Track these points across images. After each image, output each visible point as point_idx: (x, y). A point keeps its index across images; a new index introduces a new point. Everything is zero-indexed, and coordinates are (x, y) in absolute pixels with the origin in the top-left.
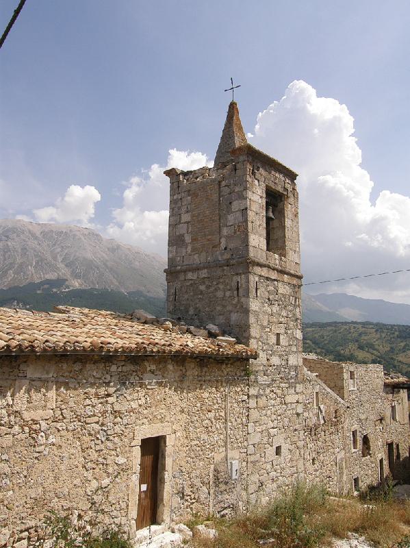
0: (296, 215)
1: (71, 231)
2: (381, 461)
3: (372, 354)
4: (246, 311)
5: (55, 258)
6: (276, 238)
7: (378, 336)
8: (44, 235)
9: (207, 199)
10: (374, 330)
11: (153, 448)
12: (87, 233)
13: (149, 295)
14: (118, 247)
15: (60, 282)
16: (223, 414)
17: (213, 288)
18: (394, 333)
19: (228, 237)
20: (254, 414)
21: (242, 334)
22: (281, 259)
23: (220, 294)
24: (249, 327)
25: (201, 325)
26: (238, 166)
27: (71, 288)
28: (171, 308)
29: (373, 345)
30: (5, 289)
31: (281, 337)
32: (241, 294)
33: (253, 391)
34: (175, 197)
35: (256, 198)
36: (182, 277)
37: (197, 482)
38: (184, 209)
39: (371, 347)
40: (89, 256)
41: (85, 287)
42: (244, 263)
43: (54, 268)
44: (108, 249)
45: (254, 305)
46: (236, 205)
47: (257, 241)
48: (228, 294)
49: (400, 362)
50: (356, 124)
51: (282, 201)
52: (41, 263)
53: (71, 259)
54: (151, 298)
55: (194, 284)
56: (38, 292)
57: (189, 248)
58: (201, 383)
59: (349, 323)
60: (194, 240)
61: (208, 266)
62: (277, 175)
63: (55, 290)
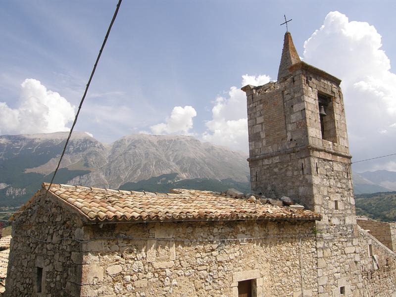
0: (343, 110)
1: (178, 139)
4: (310, 185)
5: (168, 159)
6: (328, 130)
14: (213, 148)
16: (298, 262)
19: (293, 132)
20: (322, 263)
21: (308, 203)
22: (334, 145)
24: (312, 196)
25: (277, 197)
26: (296, 78)
27: (181, 180)
28: (254, 186)
30: (136, 182)
31: (339, 203)
32: (305, 173)
33: (320, 245)
34: (251, 106)
35: (311, 100)
36: (260, 163)
40: (192, 155)
41: (191, 177)
42: (307, 150)
43: (170, 167)
44: (206, 150)
45: (316, 180)
46: (296, 108)
47: (314, 132)
48: (296, 173)
50: (383, 40)
51: (330, 101)
52: (159, 163)
53: (179, 159)
54: (240, 182)
55: (270, 168)
56: (158, 183)
57: (264, 142)
58: (280, 240)
59: (391, 193)
60: (267, 136)
61: (279, 153)
62: (326, 82)
63: (169, 181)
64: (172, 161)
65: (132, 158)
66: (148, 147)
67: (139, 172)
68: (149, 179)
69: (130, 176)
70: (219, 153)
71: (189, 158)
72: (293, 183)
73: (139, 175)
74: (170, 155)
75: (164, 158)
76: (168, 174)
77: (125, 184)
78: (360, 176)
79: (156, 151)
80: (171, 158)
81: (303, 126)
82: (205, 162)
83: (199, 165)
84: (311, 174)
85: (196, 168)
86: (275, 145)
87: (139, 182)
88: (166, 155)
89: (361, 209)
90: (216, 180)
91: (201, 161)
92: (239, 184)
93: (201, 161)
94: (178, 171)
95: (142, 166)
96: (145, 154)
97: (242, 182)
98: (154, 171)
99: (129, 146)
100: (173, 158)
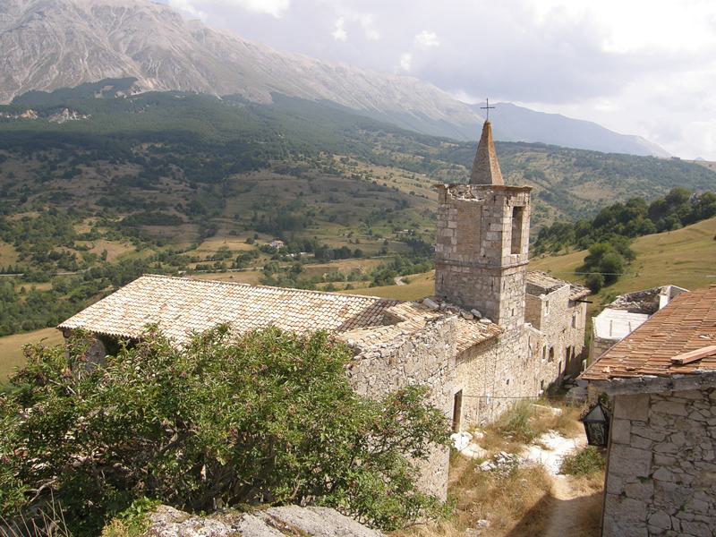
2: (560, 363)
3: (542, 185)
4: (498, 302)
7: (550, 162)
8: (96, 13)
9: (471, 217)
10: (546, 154)
11: (458, 397)
12: (159, 10)
13: (251, 100)
14: (207, 32)
15: (127, 82)
17: (473, 282)
18: (570, 160)
20: (498, 365)
23: (478, 286)
25: (468, 309)
26: (497, 197)
27: (143, 91)
28: (439, 288)
29: (543, 174)
30: (48, 91)
32: (494, 290)
35: (508, 220)
37: (472, 409)
38: (450, 218)
39: (540, 177)
40: (165, 44)
43: (119, 63)
44: (193, 35)
45: (503, 296)
46: (493, 227)
47: (506, 251)
48: (485, 287)
49: (574, 196)
52: (97, 54)
53: (140, 50)
54: (255, 103)
55: (458, 275)
56: (97, 96)
57: (455, 249)
59: (515, 144)
60: (458, 244)
63: (120, 94)
64: (124, 52)
65: (36, 38)
66: (72, 19)
67: (54, 72)
68: (77, 87)
69: (36, 79)
70: (218, 44)
71: (159, 48)
72: (481, 295)
73: (54, 76)
74: (121, 39)
75: (106, 44)
76: (116, 79)
77: (26, 94)
78: (470, 111)
79: (90, 30)
80: (121, 45)
81: (498, 246)
82: (191, 60)
83: (180, 65)
84: (499, 292)
85: (174, 70)
86: (466, 256)
87: (56, 92)
88: (111, 39)
89: (464, 168)
90: (211, 96)
91: (182, 56)
92: (255, 106)
93: (182, 56)
94: (137, 73)
95: (61, 59)
96: (66, 34)
97: (261, 103)
98: (86, 71)
99: (27, 11)
100: (128, 45)
